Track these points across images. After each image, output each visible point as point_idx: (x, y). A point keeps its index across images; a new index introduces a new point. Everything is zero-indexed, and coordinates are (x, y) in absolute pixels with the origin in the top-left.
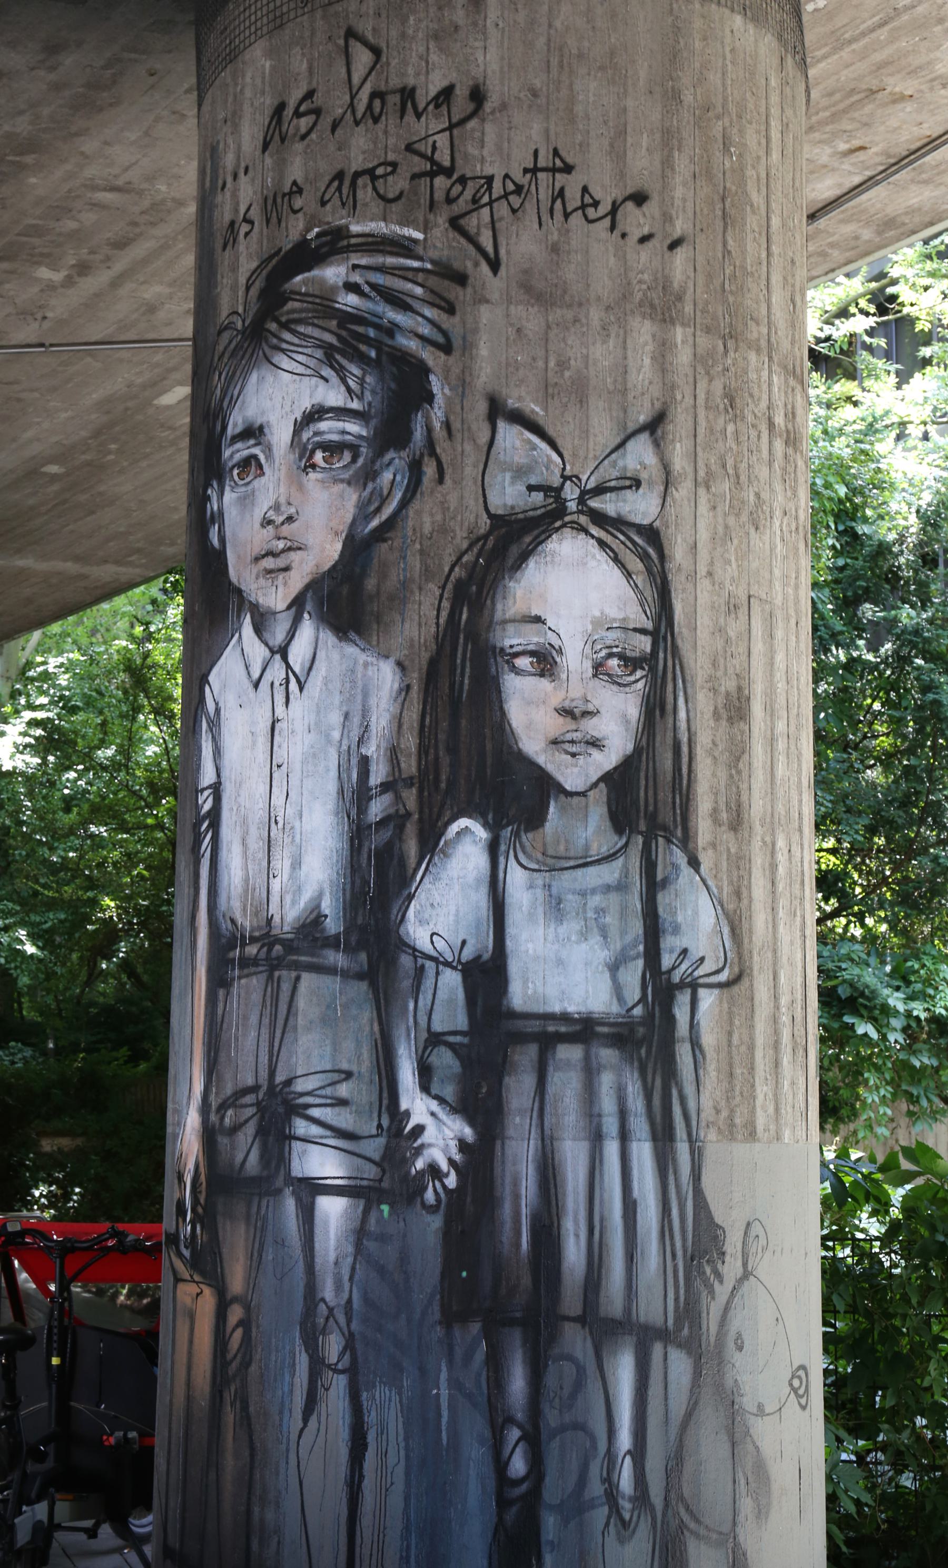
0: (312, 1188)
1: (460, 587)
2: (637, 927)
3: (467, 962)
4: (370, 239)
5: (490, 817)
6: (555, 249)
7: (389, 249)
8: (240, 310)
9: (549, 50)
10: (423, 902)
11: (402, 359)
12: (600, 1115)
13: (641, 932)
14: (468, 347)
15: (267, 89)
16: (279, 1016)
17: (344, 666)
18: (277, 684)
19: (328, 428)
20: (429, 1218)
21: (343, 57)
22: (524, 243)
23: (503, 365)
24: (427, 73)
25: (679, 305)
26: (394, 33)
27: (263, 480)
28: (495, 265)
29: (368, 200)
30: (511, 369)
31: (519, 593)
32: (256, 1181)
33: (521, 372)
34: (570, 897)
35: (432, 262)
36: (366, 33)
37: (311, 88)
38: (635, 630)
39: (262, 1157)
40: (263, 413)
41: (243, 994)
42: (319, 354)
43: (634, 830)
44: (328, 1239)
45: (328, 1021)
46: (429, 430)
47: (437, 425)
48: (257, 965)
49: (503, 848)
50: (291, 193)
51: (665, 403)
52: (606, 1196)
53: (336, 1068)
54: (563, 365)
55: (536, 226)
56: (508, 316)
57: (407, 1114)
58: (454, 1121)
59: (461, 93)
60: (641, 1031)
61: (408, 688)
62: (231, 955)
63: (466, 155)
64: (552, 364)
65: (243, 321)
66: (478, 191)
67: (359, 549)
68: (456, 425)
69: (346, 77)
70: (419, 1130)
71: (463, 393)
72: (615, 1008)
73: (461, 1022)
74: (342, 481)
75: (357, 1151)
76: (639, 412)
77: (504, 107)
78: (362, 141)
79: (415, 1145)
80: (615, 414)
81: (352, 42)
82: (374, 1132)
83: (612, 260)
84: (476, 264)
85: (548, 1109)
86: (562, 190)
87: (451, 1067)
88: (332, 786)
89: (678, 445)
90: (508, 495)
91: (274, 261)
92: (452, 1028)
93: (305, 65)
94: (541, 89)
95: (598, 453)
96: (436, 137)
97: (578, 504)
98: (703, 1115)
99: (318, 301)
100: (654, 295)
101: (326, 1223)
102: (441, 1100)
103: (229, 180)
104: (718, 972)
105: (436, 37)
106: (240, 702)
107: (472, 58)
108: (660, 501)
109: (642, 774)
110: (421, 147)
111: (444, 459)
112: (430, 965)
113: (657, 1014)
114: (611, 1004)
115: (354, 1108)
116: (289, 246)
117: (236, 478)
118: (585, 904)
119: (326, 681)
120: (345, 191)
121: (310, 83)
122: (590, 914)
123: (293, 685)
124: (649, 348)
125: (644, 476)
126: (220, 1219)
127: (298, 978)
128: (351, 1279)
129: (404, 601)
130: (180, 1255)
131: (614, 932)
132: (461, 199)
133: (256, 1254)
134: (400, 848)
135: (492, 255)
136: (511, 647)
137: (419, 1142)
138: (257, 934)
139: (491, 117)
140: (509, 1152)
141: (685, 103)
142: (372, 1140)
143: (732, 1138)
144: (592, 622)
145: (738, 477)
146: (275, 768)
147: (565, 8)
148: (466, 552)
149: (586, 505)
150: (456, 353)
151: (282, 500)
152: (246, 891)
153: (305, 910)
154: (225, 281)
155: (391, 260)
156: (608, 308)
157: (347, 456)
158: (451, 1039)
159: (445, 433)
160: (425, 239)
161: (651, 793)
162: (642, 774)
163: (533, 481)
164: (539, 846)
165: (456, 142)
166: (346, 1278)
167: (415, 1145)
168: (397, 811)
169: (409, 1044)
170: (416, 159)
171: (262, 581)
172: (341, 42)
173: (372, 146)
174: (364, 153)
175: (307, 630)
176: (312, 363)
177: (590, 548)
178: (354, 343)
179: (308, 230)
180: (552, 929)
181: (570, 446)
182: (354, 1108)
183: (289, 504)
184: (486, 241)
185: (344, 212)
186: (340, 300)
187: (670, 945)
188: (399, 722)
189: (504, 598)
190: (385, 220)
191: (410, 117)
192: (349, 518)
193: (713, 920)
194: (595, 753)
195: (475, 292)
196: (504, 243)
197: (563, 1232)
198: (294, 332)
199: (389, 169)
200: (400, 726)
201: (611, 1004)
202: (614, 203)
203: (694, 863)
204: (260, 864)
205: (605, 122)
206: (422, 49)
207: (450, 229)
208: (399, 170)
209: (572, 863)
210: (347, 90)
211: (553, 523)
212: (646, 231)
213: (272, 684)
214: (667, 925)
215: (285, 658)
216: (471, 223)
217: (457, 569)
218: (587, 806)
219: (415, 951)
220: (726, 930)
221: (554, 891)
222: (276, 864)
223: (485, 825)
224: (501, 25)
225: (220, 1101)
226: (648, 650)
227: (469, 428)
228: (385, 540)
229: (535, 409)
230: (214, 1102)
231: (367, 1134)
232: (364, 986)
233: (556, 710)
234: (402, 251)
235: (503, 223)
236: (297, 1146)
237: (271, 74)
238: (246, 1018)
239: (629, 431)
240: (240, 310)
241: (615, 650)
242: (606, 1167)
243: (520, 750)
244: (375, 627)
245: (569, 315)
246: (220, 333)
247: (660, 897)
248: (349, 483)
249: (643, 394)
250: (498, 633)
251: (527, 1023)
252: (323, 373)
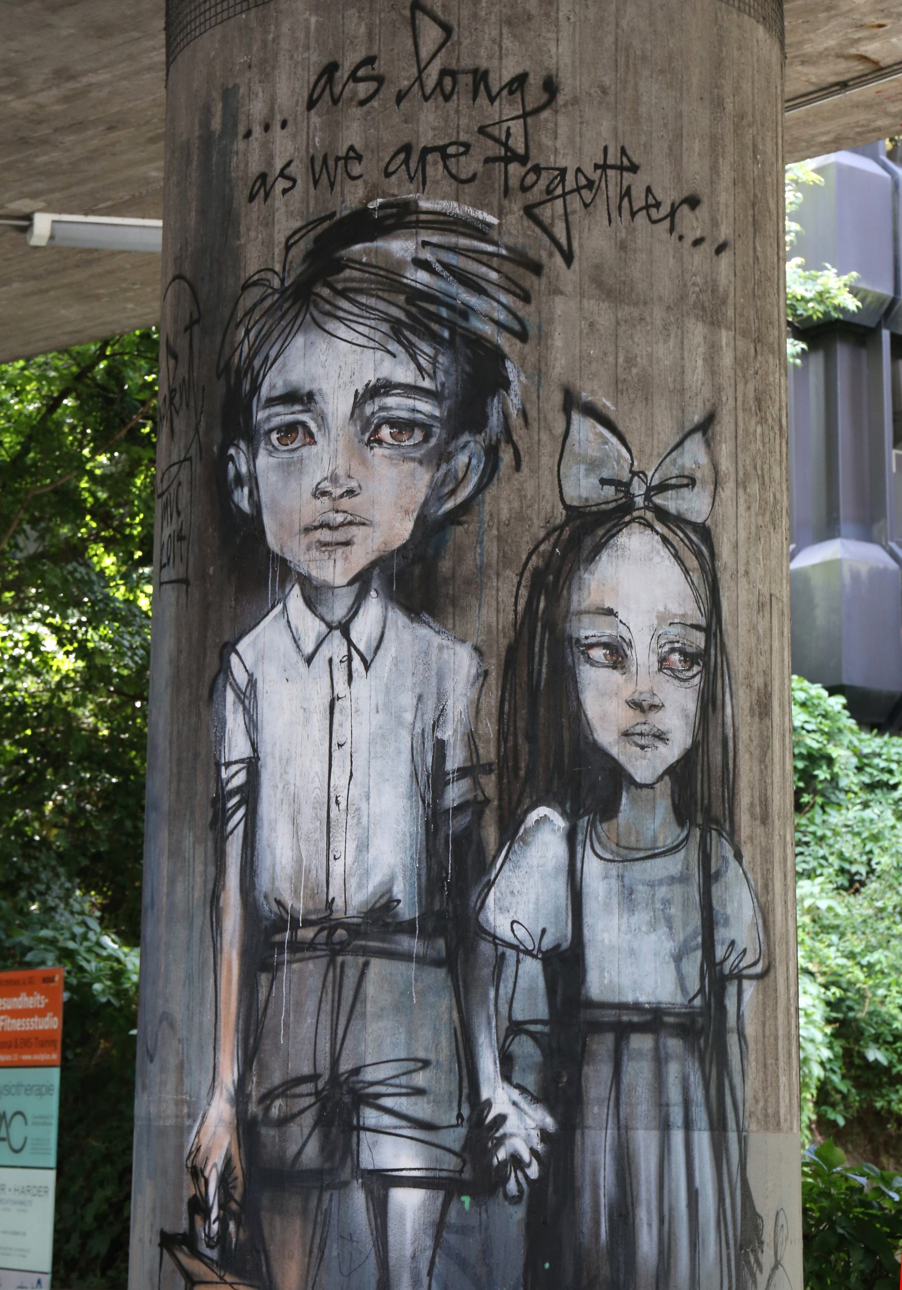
0: (382, 1182)
1: (538, 574)
2: (696, 919)
3: (547, 951)
4: (442, 218)
5: (568, 806)
6: (622, 246)
7: (462, 230)
8: (278, 268)
9: (616, 49)
10: (503, 889)
11: (477, 341)
12: (668, 1105)
13: (699, 923)
14: (543, 337)
15: (313, 44)
16: (343, 1002)
17: (416, 648)
18: (336, 661)
19: (397, 405)
20: (512, 1209)
21: (410, 29)
22: (595, 238)
23: (577, 357)
24: (501, 58)
25: (723, 308)
26: (465, 13)
27: (314, 449)
28: (568, 258)
29: (439, 177)
30: (584, 362)
31: (594, 585)
32: (318, 1173)
33: (594, 366)
34: (640, 888)
35: (507, 248)
36: (435, 8)
37: (372, 54)
38: (693, 626)
39: (322, 1148)
40: (313, 380)
41: (295, 979)
42: (385, 327)
43: (693, 824)
44: (404, 1232)
45: (402, 1007)
46: (506, 416)
47: (513, 412)
48: (315, 949)
49: (580, 837)
50: (347, 158)
51: (714, 404)
52: (673, 1185)
53: (412, 1056)
54: (630, 361)
55: (606, 222)
56: (581, 309)
57: (489, 1104)
58: (536, 1110)
59: (535, 82)
60: (700, 1020)
61: (486, 673)
62: (278, 938)
63: (540, 146)
64: (621, 360)
65: (282, 281)
66: (552, 182)
67: (431, 530)
68: (533, 414)
69: (413, 49)
70: (501, 1119)
71: (539, 382)
72: (679, 999)
73: (542, 1010)
74: (413, 459)
75: (436, 1141)
76: (694, 413)
77: (575, 101)
78: (431, 117)
79: (497, 1135)
80: (675, 413)
81: (419, 15)
82: (454, 1121)
83: (672, 261)
84: (551, 255)
85: (623, 1098)
86: (629, 188)
87: (532, 1056)
88: (404, 769)
89: (724, 446)
90: (583, 487)
91: (326, 225)
92: (534, 1017)
93: (363, 29)
94: (610, 87)
95: (661, 451)
96: (510, 123)
97: (645, 500)
98: (747, 1105)
99: (382, 273)
100: (705, 298)
101: (402, 1216)
102: (523, 1089)
103: (257, 131)
104: (755, 964)
105: (509, 23)
106: (286, 675)
107: (545, 49)
108: (710, 500)
109: (699, 768)
110: (495, 131)
111: (521, 446)
112: (510, 953)
113: (713, 1005)
114: (676, 994)
115: (432, 1098)
116: (346, 213)
117: (276, 443)
118: (654, 895)
119: (396, 662)
120: (413, 165)
121: (370, 48)
122: (658, 906)
123: (357, 663)
124: (701, 350)
125: (698, 475)
126: (265, 1217)
127: (366, 964)
128: (430, 1273)
129: (481, 587)
130: (200, 1256)
131: (678, 924)
132: (535, 188)
133: (316, 1250)
134: (479, 835)
135: (566, 248)
136: (587, 638)
137: (501, 1132)
138: (313, 917)
139: (563, 110)
140: (588, 1142)
141: (727, 111)
142: (452, 1130)
143: (767, 1129)
144: (657, 617)
145: (763, 477)
146: (335, 747)
147: (631, 9)
148: (543, 540)
149: (651, 501)
150: (532, 342)
151: (341, 472)
152: (298, 872)
153: (374, 894)
154: (253, 234)
155: (464, 242)
156: (669, 308)
157: (418, 436)
158: (532, 1028)
159: (521, 421)
160: (500, 225)
161: (706, 786)
162: (699, 768)
163: (606, 474)
164: (613, 836)
165: (530, 131)
166: (424, 1272)
167: (497, 1135)
168: (475, 796)
169: (490, 1032)
170: (490, 143)
171: (314, 553)
172: (407, 13)
173: (442, 124)
174: (434, 129)
175: (373, 610)
176: (378, 336)
177: (655, 543)
178: (426, 321)
179: (370, 199)
180: (625, 919)
181: (637, 442)
182: (432, 1098)
183: (349, 477)
184: (560, 232)
185: (412, 187)
186: (408, 275)
187: (722, 934)
189: (580, 589)
190: (457, 200)
191: (483, 99)
192: (421, 497)
193: (751, 913)
194: (660, 745)
195: (550, 282)
196: (577, 236)
197: (637, 1221)
199: (462, 149)
200: (478, 712)
201: (676, 994)
202: (673, 205)
203: (738, 856)
204: (316, 845)
205: (665, 125)
206: (495, 33)
207: (525, 217)
208: (471, 152)
209: (642, 854)
210: (414, 62)
211: (623, 517)
212: (698, 234)
213: (330, 661)
214: (719, 916)
215: (346, 634)
216: (546, 213)
217: (534, 558)
218: (654, 798)
219: (495, 939)
220: (760, 922)
221: (627, 881)
222: (338, 845)
223: (563, 814)
224: (572, 20)
225: (263, 1090)
226: (703, 646)
227: (545, 418)
228: (460, 523)
229: (606, 403)
230: (254, 1091)
231: (445, 1124)
232: (441, 973)
233: (627, 702)
234: (476, 234)
235: (576, 216)
237: (317, 30)
238: (299, 1004)
239: (687, 430)
240: (278, 268)
241: (676, 645)
242: (673, 1157)
243: (595, 741)
244: (451, 610)
245: (636, 313)
246: (245, 287)
247: (714, 889)
248: (421, 462)
249: (697, 395)
250: (574, 623)
251: (604, 1012)
252: (390, 348)
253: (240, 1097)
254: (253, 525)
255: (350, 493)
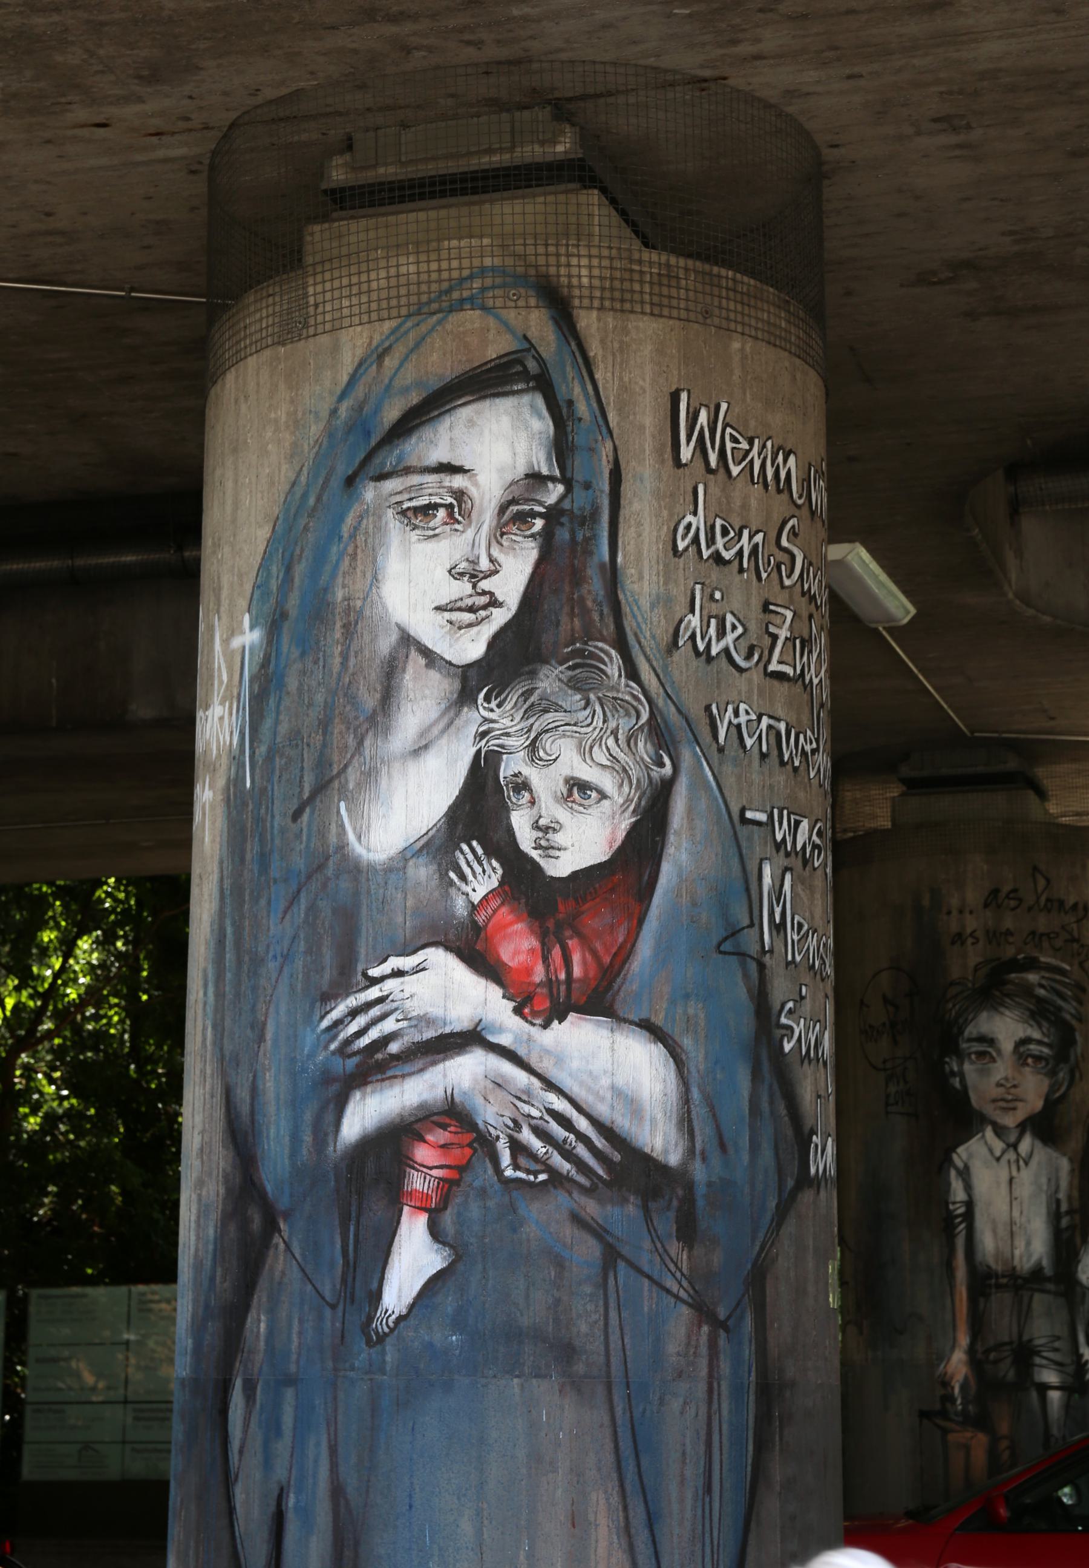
42: (1027, 1013)
59: (1081, 906)
67: (1051, 1105)
88: (1043, 1210)
103: (955, 913)
119: (1039, 1163)
123: (1021, 1163)
155: (1058, 977)
157: (1043, 1063)
171: (998, 1112)
175: (1026, 1144)
188: (1071, 1184)
198: (1012, 1000)
222: (1017, 1243)
236: (1036, 1369)
240: (970, 978)
246: (952, 984)
253: (971, 1351)
254: (963, 1095)
255: (1015, 1086)
